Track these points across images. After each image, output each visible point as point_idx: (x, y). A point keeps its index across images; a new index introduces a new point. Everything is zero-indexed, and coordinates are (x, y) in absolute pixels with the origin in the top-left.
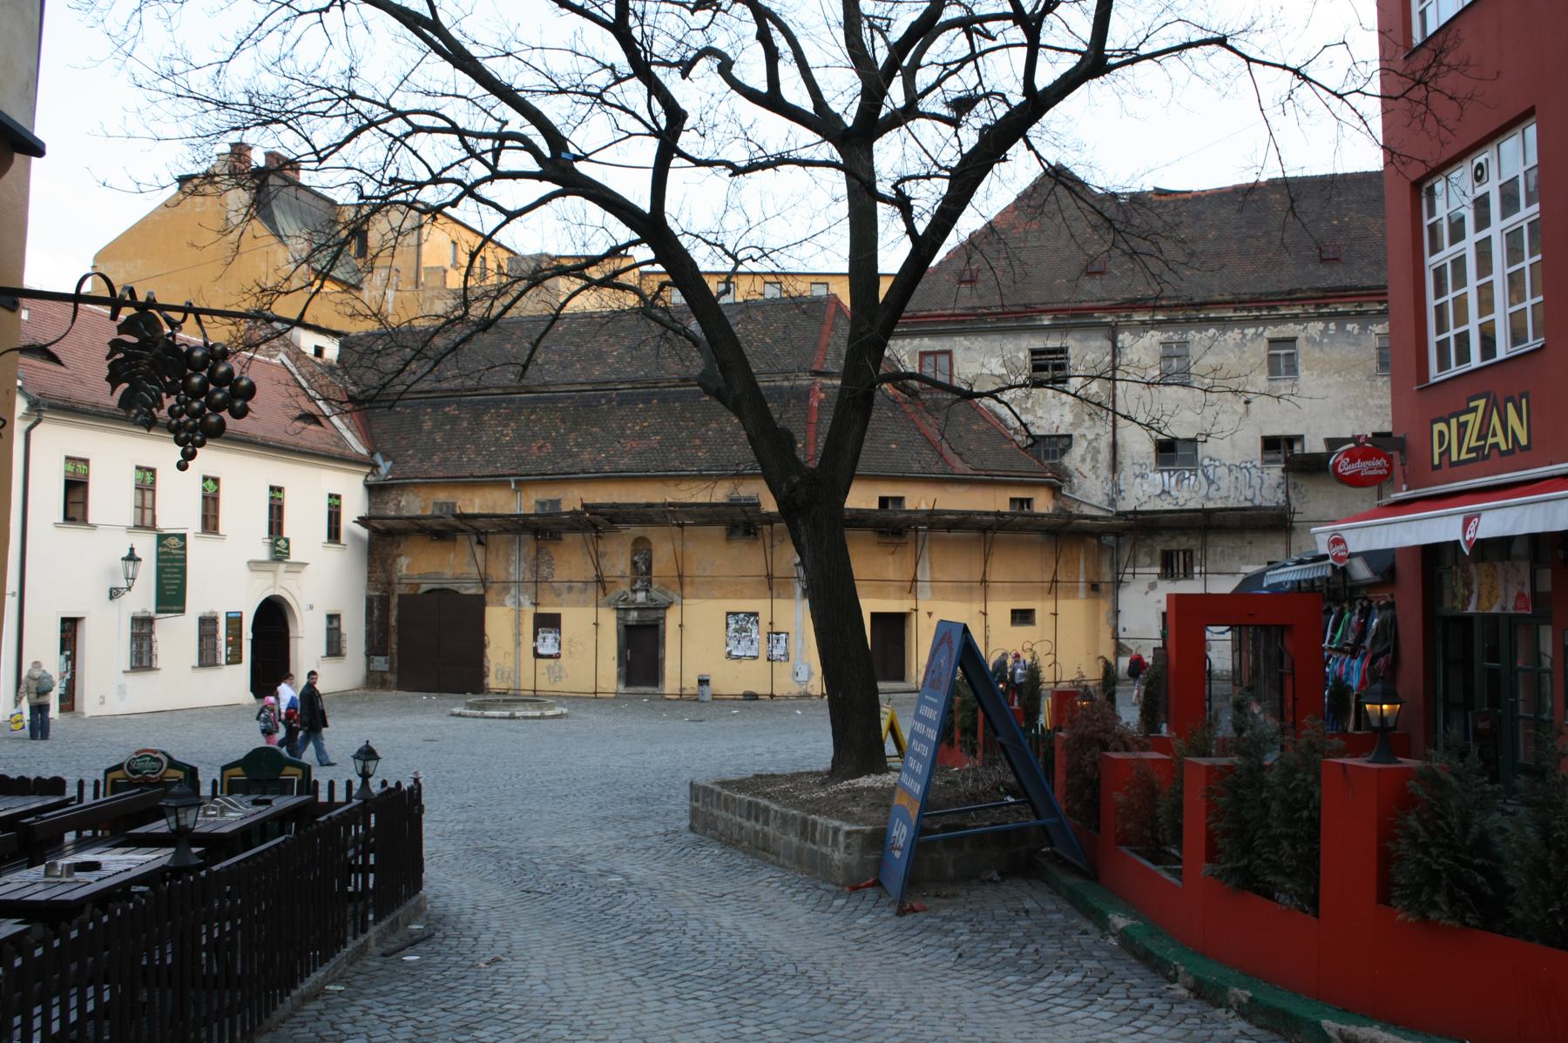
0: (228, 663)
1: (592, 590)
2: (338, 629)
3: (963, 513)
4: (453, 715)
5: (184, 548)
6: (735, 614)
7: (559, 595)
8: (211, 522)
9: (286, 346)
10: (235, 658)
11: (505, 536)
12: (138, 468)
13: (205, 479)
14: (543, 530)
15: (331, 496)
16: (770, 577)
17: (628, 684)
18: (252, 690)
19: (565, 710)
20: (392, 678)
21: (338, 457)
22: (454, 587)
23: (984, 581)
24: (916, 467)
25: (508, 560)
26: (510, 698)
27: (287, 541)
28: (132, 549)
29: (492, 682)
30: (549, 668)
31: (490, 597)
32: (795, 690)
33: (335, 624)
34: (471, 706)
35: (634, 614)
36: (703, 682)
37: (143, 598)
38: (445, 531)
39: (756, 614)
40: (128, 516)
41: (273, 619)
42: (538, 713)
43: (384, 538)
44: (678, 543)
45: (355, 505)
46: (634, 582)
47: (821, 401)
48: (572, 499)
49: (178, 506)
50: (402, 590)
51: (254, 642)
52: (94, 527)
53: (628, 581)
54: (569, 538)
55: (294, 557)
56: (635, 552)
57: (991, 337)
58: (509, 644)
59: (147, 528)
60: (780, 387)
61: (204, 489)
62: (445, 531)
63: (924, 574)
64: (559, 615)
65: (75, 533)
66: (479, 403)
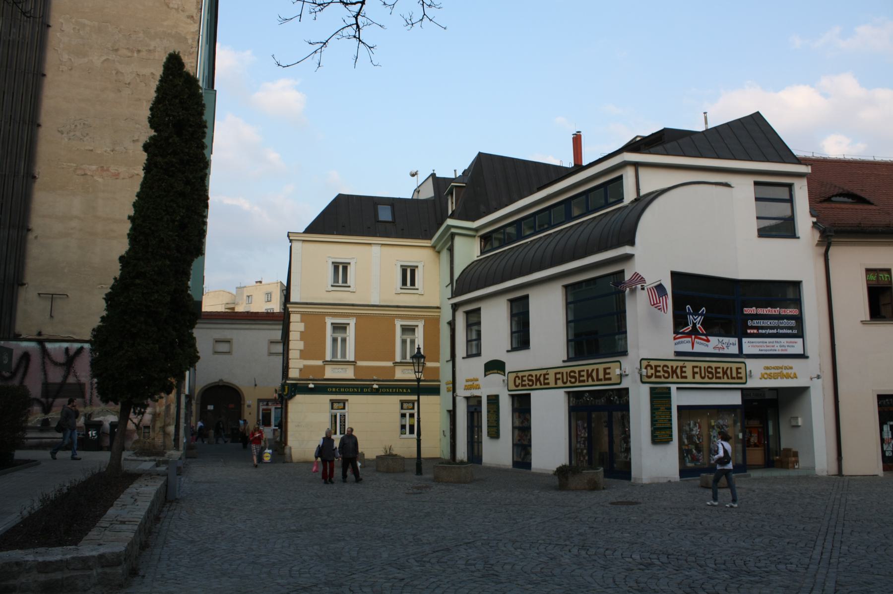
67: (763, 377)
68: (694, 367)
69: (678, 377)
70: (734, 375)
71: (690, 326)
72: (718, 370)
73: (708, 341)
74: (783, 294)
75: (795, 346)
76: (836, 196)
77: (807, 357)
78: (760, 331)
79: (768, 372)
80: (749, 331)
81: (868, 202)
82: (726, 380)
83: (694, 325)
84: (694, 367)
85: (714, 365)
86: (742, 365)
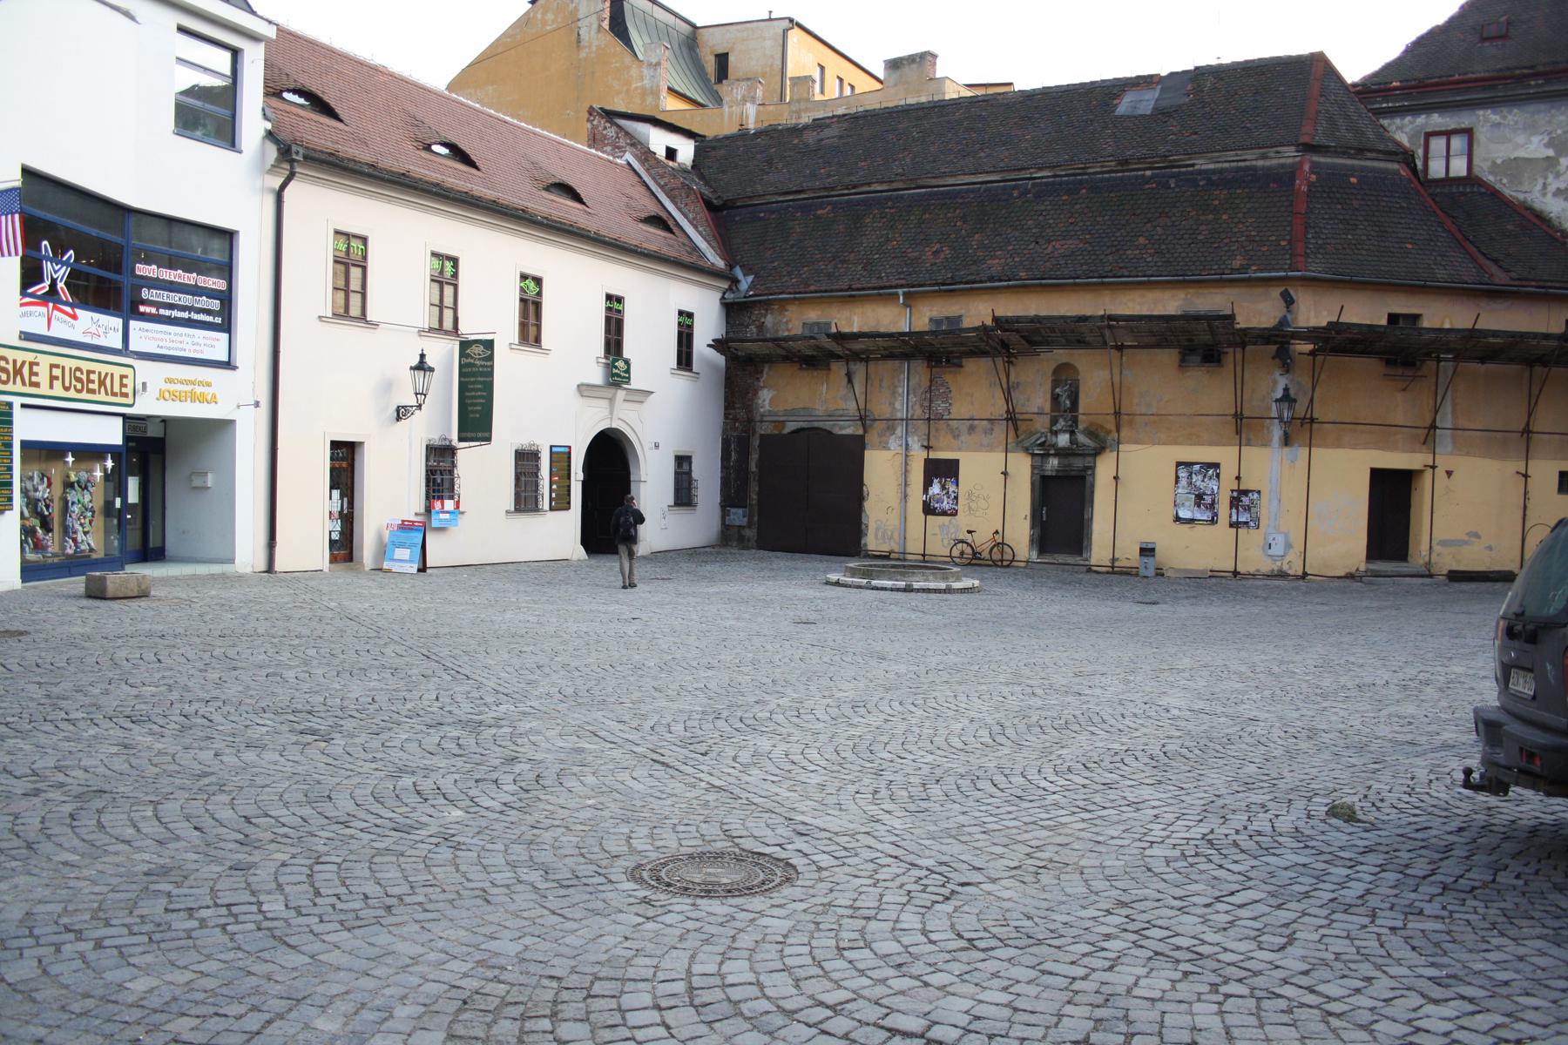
0: (551, 509)
1: (1000, 428)
2: (689, 473)
3: (1513, 335)
4: (828, 583)
5: (491, 358)
6: (1188, 465)
7: (957, 436)
8: (532, 331)
9: (633, 145)
10: (561, 503)
11: (890, 364)
12: (434, 254)
13: (524, 277)
14: (937, 352)
15: (681, 313)
16: (1238, 416)
17: (1042, 550)
18: (584, 543)
19: (977, 583)
20: (751, 533)
21: (688, 265)
22: (827, 426)
23: (1527, 431)
24: (1441, 273)
25: (894, 393)
26: (895, 563)
27: (627, 362)
28: (422, 356)
29: (872, 542)
30: (941, 527)
31: (872, 438)
32: (1266, 566)
33: (685, 467)
34: (853, 572)
35: (1054, 462)
36: (1147, 551)
37: (438, 417)
38: (818, 355)
39: (1216, 466)
40: (424, 316)
41: (610, 456)
42: (943, 585)
43: (744, 362)
44: (1116, 371)
45: (708, 327)
46: (1054, 421)
47: (1310, 185)
48: (977, 312)
49: (489, 311)
50: (765, 429)
51: (586, 485)
52: (375, 325)
53: (1046, 420)
54: (971, 365)
55: (635, 383)
56: (1056, 383)
57: (1532, 107)
58: (893, 498)
59: (447, 332)
60: (1254, 168)
61: (522, 290)
62: (818, 355)
63: (1446, 419)
64: (957, 461)
65: (349, 333)
66: (858, 203)
67: (161, 396)
68: (52, 366)
69: (24, 383)
70: (117, 389)
71: (47, 283)
72: (92, 377)
73: (74, 317)
74: (209, 248)
75: (212, 345)
76: (289, 91)
77: (235, 368)
78: (162, 312)
79: (172, 387)
80: (142, 309)
81: (472, 164)
82: (102, 397)
83: (54, 282)
84: (52, 366)
85: (86, 366)
86: (129, 371)
